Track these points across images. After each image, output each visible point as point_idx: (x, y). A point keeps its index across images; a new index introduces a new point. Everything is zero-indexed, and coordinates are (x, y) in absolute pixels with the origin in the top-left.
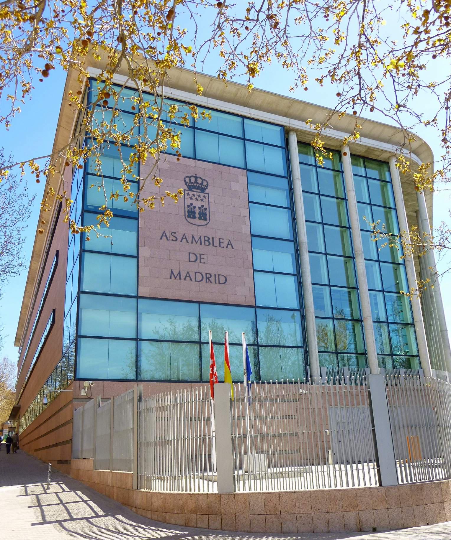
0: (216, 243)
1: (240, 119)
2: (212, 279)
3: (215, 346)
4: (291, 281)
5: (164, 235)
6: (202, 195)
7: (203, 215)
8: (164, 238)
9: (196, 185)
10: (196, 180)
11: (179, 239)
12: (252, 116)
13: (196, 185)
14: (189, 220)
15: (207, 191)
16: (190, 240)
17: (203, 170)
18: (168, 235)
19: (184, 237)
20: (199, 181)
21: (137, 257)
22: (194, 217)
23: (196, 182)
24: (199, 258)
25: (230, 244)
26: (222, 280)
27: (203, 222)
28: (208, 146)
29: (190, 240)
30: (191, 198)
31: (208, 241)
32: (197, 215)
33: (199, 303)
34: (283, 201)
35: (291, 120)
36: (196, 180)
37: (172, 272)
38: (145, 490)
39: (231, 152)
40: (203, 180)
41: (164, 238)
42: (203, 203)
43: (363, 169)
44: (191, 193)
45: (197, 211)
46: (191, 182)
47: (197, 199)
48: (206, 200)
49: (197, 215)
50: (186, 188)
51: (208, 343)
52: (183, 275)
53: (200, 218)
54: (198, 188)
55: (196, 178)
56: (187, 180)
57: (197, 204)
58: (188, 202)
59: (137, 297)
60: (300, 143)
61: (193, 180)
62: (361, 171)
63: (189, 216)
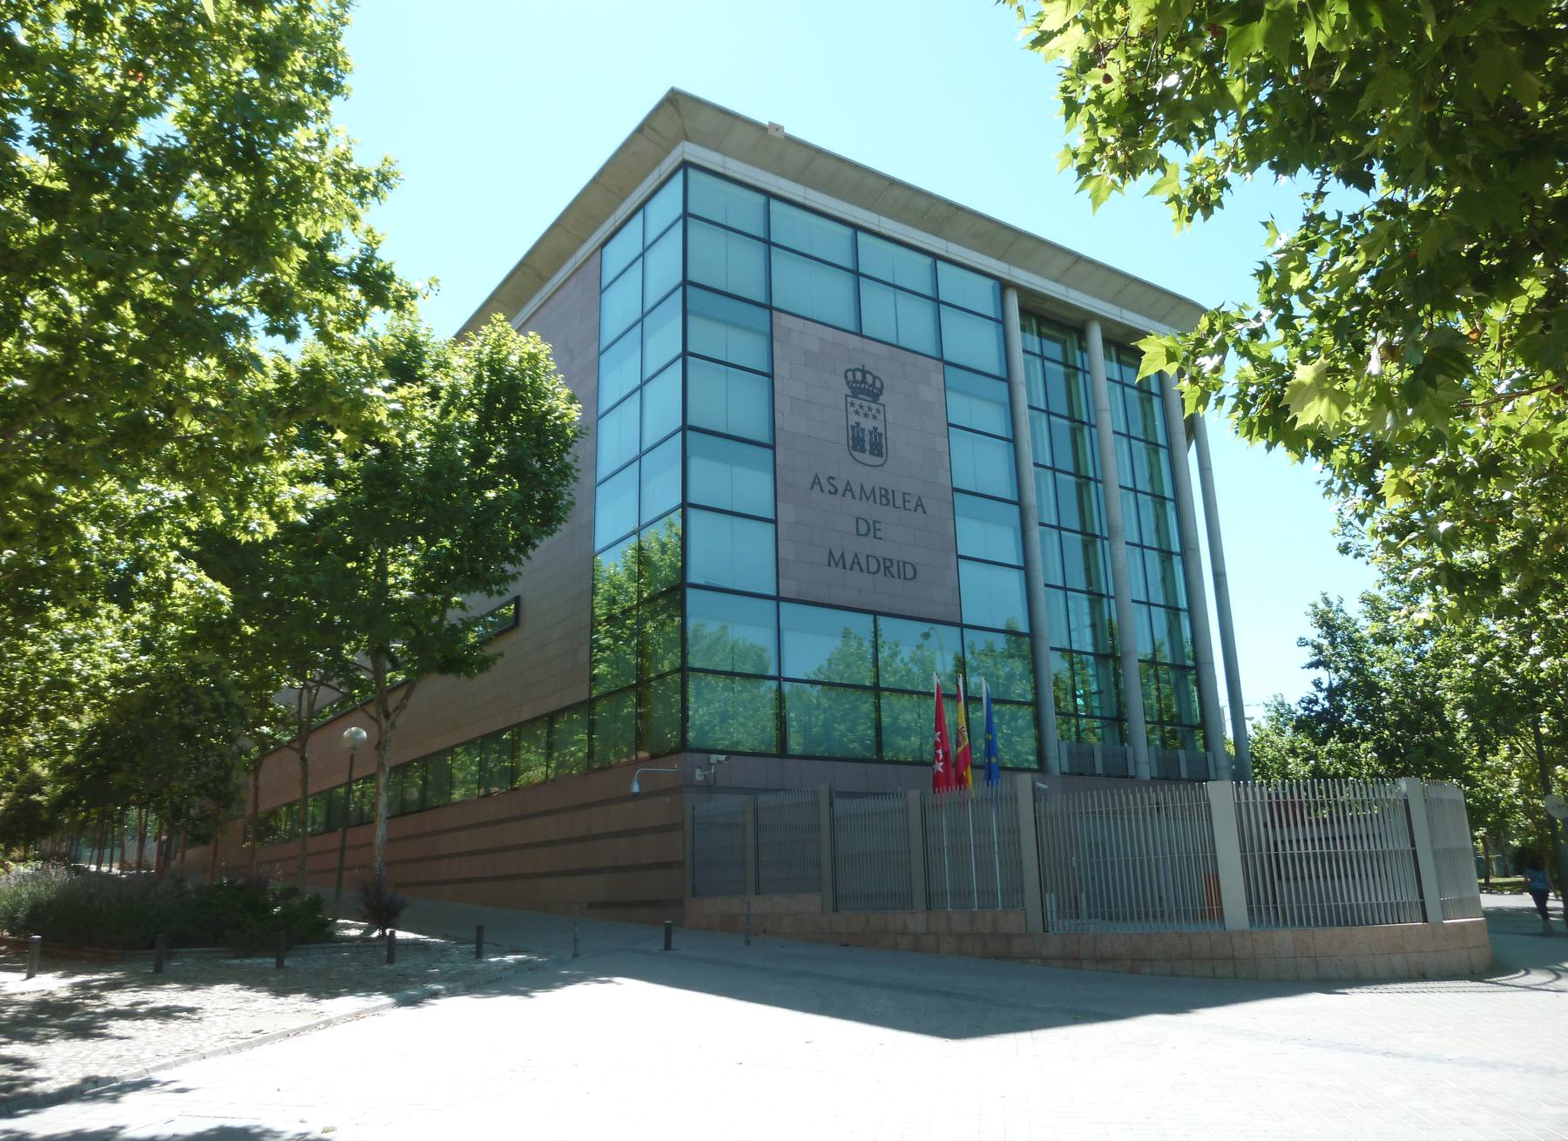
0: (899, 502)
1: (760, 199)
2: (894, 570)
3: (996, 708)
4: (1014, 579)
5: (816, 481)
6: (874, 406)
7: (877, 448)
8: (817, 487)
9: (864, 387)
10: (864, 377)
11: (841, 490)
12: (808, 203)
13: (864, 387)
14: (856, 454)
15: (882, 399)
16: (857, 492)
17: (878, 361)
18: (824, 482)
19: (848, 488)
20: (869, 379)
21: (775, 522)
22: (863, 450)
23: (864, 381)
24: (872, 529)
25: (920, 504)
26: (910, 573)
27: (878, 461)
28: (881, 313)
29: (857, 492)
30: (857, 413)
31: (885, 497)
32: (867, 446)
33: (876, 614)
34: (998, 425)
35: (728, 160)
36: (864, 377)
37: (831, 554)
38: (510, 959)
39: (914, 325)
40: (875, 378)
41: (817, 487)
42: (876, 424)
43: (1036, 339)
44: (857, 402)
45: (867, 439)
46: (855, 381)
47: (866, 415)
48: (881, 417)
49: (867, 446)
50: (849, 392)
51: (980, 699)
52: (849, 559)
53: (872, 453)
54: (868, 393)
55: (864, 373)
56: (850, 374)
57: (867, 424)
58: (854, 419)
59: (778, 599)
60: (1107, 342)
61: (859, 376)
62: (1034, 343)
63: (855, 449)
